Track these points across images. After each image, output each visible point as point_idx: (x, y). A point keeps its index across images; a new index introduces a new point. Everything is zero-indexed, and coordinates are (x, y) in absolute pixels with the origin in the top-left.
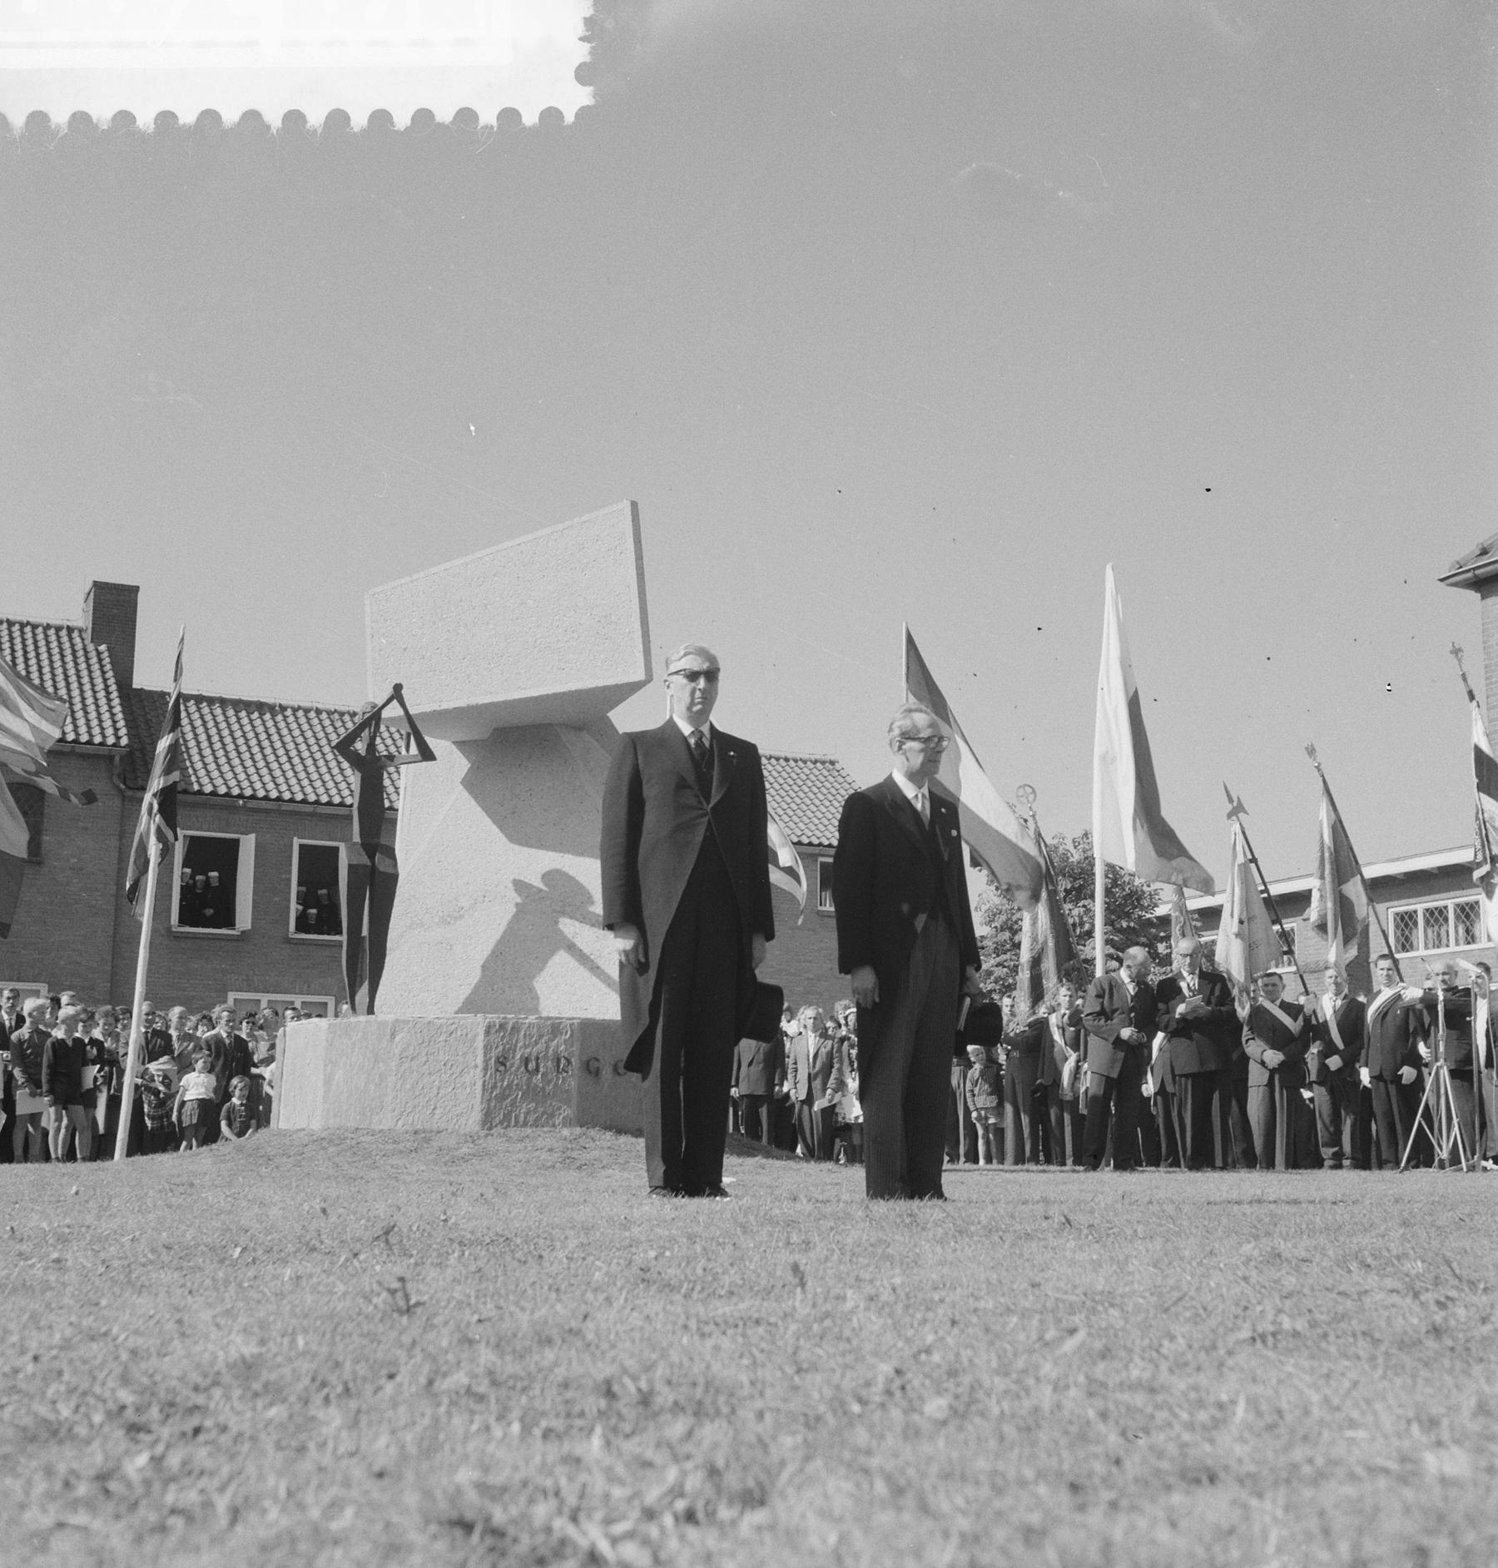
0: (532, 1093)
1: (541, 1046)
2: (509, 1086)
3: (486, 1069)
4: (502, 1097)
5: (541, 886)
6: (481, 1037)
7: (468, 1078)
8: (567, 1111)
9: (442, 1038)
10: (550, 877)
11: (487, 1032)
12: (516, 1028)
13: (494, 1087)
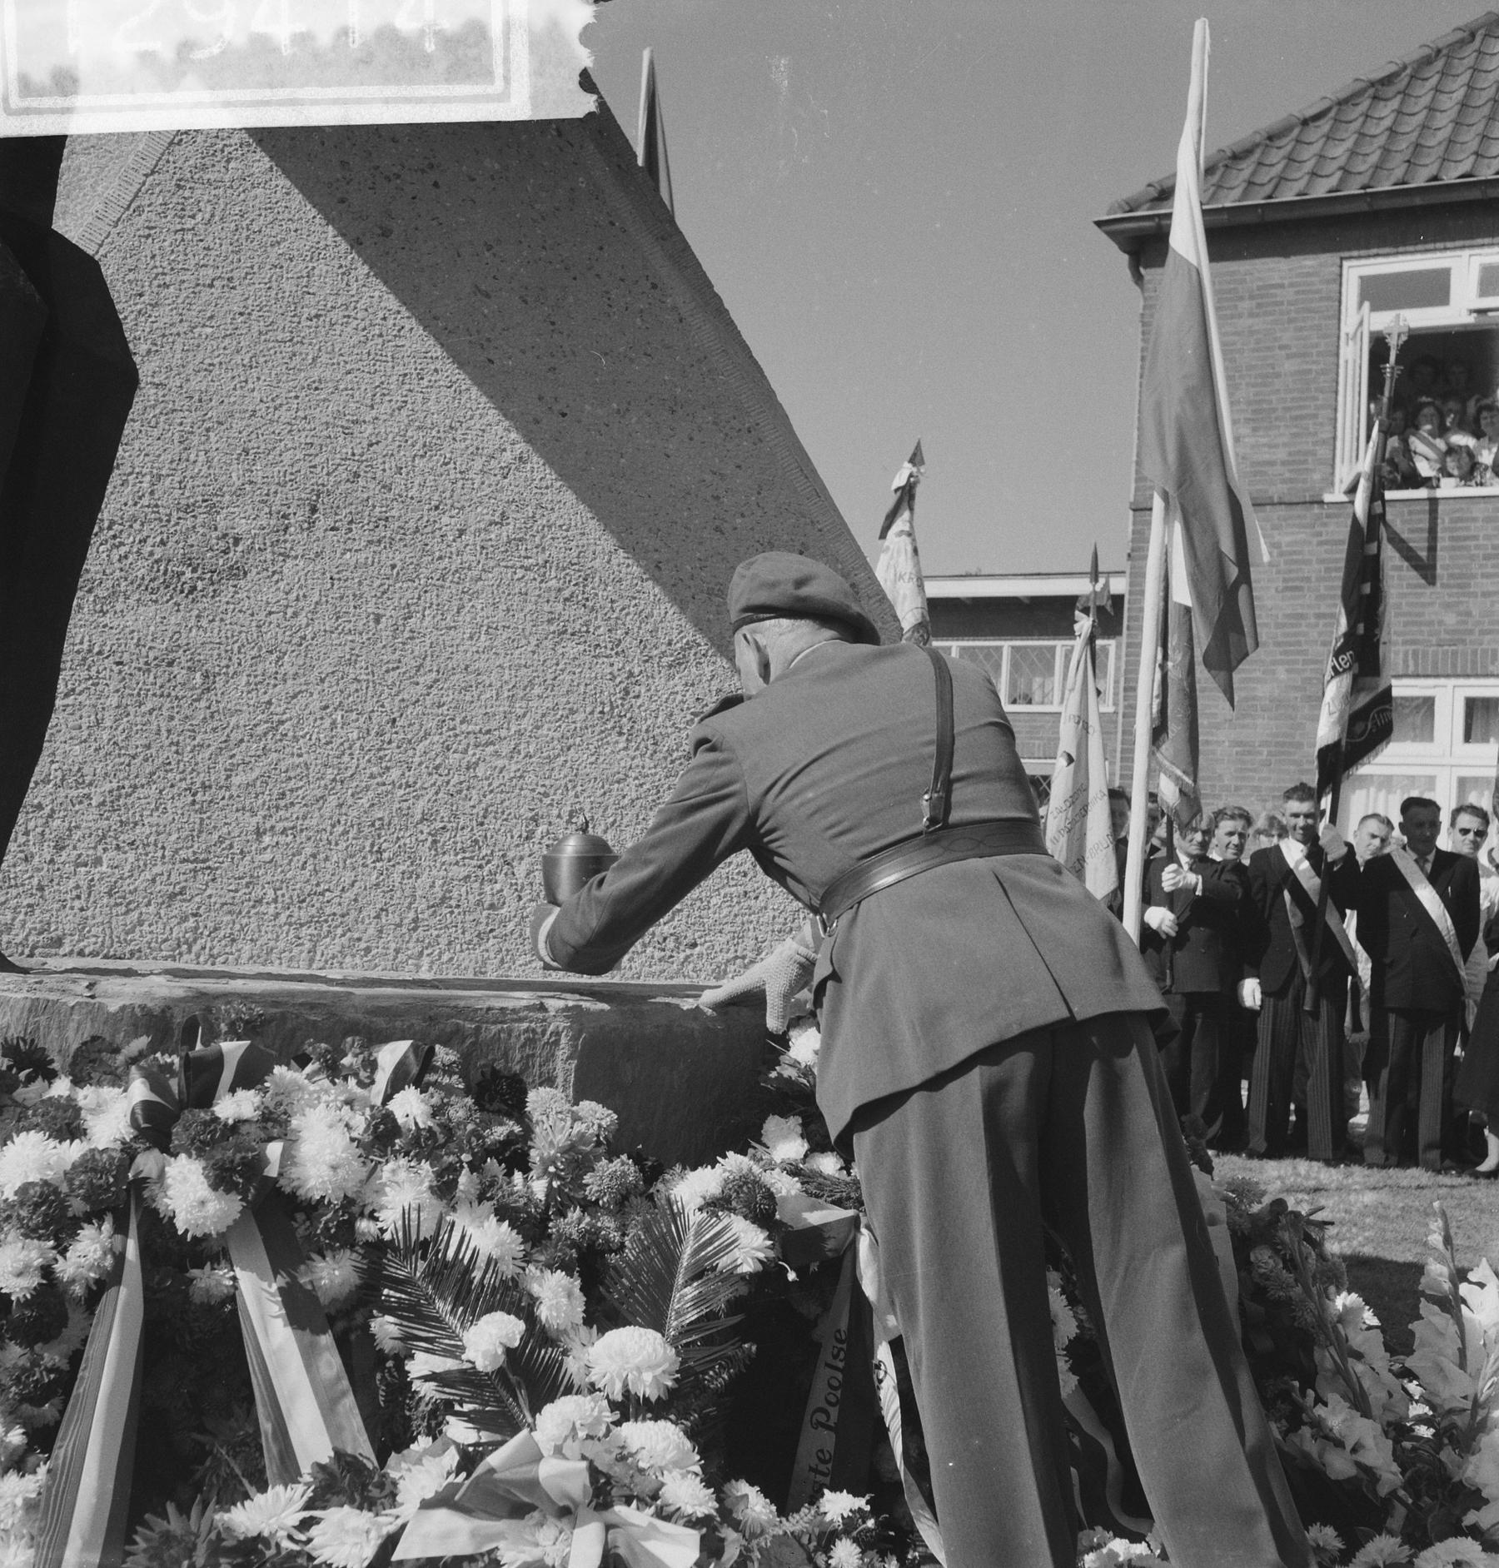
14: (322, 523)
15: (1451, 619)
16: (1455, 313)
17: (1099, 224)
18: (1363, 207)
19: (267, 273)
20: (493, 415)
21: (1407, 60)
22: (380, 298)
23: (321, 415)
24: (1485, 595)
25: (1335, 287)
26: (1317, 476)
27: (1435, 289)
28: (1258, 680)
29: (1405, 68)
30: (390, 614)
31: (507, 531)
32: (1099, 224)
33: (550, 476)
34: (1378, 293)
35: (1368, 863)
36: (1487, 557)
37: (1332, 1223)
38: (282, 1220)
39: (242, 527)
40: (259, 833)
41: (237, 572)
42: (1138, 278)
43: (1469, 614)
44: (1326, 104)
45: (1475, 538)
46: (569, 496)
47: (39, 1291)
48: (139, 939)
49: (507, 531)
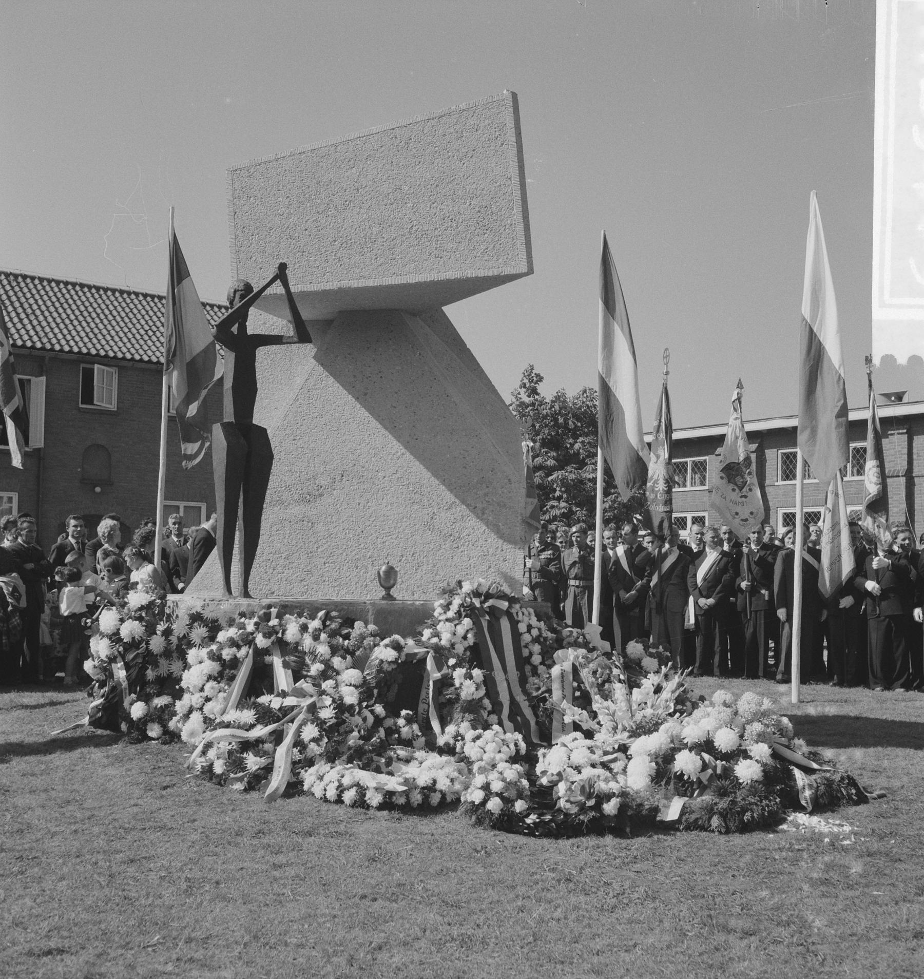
14: (345, 479)
19: (331, 412)
20: (395, 442)
22: (364, 413)
23: (345, 449)
30: (363, 502)
31: (398, 475)
33: (412, 457)
38: (282, 645)
39: (323, 483)
40: (325, 564)
41: (321, 495)
46: (417, 463)
47: (231, 659)
48: (293, 592)
49: (398, 475)
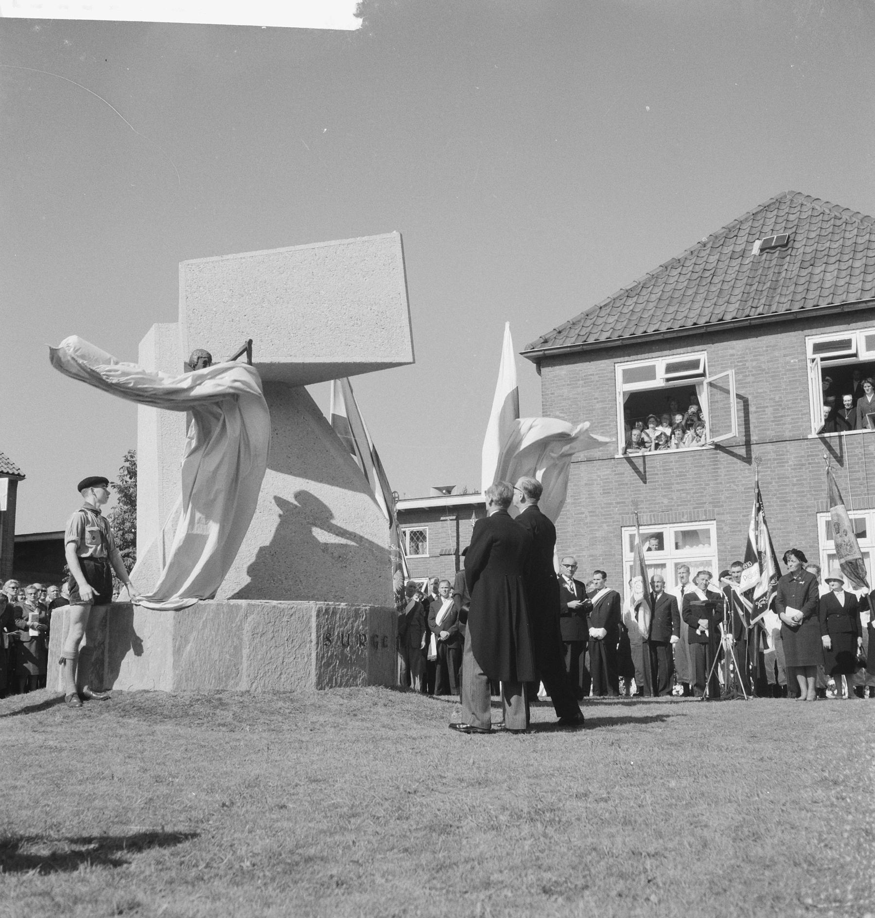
0: (345, 662)
1: (349, 626)
2: (332, 655)
3: (317, 643)
4: (328, 664)
5: (296, 503)
6: (314, 619)
7: (305, 651)
8: (364, 675)
9: (285, 619)
10: (299, 495)
11: (318, 616)
12: (334, 613)
13: (323, 657)
15: (666, 501)
16: (658, 382)
17: (521, 354)
18: (618, 343)
21: (641, 280)
24: (678, 491)
25: (704, 517)
26: (612, 448)
27: (649, 373)
28: (597, 530)
29: (640, 283)
32: (521, 354)
34: (629, 376)
35: (823, 596)
36: (677, 476)
37: (453, 726)
42: (539, 372)
43: (672, 499)
44: (609, 300)
45: (672, 469)
